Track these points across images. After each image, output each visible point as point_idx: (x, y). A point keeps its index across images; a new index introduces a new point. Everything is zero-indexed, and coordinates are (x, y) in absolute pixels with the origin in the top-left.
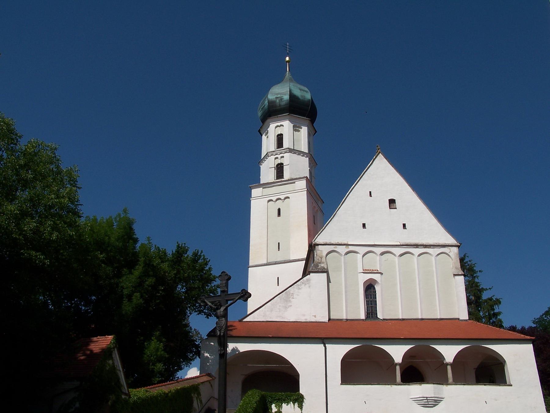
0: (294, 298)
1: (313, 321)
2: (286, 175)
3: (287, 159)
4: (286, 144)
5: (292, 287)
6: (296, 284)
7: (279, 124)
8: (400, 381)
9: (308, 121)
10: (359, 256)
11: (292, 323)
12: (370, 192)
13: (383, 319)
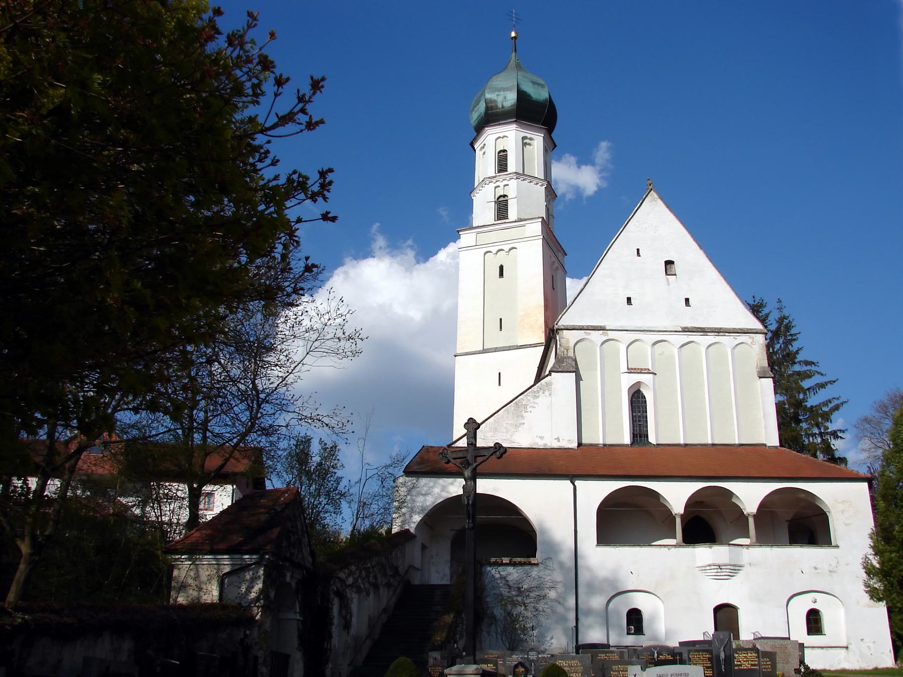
0: (528, 412)
1: (556, 447)
2: (513, 214)
3: (512, 188)
4: (512, 166)
5: (526, 393)
6: (530, 390)
7: (501, 135)
8: (682, 541)
9: (545, 131)
10: (622, 348)
11: (526, 451)
12: (638, 250)
13: (657, 444)
